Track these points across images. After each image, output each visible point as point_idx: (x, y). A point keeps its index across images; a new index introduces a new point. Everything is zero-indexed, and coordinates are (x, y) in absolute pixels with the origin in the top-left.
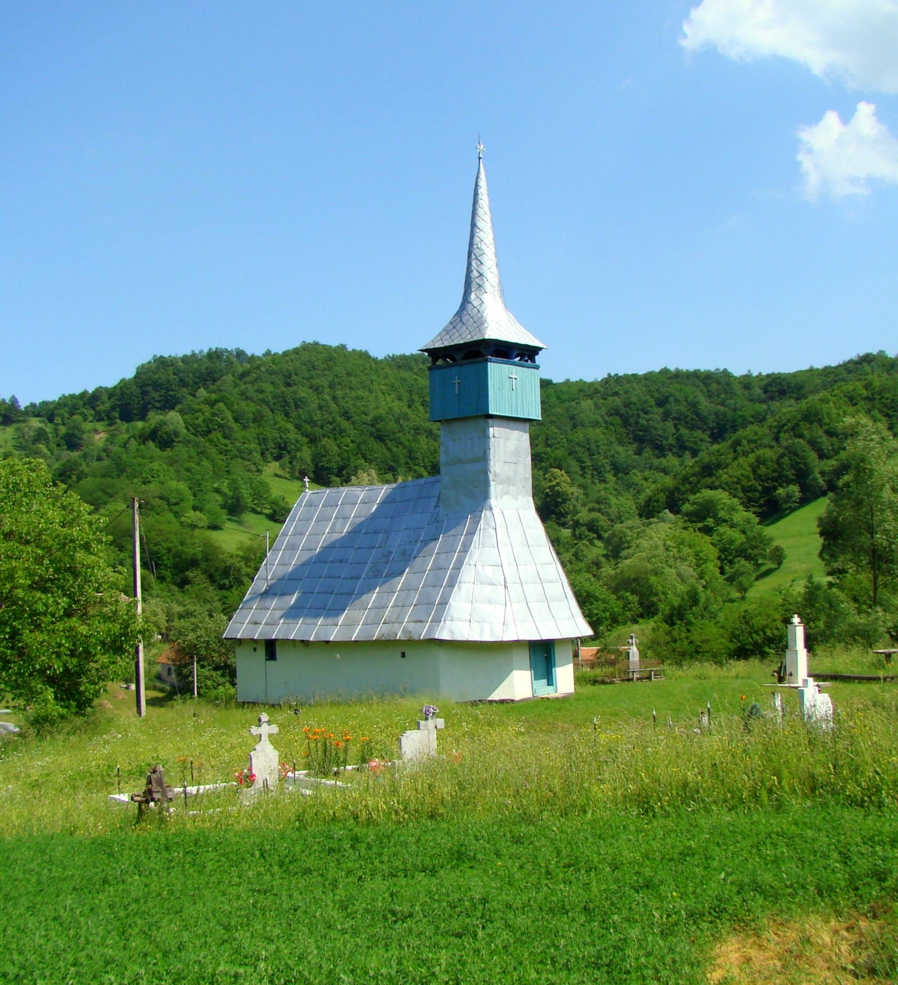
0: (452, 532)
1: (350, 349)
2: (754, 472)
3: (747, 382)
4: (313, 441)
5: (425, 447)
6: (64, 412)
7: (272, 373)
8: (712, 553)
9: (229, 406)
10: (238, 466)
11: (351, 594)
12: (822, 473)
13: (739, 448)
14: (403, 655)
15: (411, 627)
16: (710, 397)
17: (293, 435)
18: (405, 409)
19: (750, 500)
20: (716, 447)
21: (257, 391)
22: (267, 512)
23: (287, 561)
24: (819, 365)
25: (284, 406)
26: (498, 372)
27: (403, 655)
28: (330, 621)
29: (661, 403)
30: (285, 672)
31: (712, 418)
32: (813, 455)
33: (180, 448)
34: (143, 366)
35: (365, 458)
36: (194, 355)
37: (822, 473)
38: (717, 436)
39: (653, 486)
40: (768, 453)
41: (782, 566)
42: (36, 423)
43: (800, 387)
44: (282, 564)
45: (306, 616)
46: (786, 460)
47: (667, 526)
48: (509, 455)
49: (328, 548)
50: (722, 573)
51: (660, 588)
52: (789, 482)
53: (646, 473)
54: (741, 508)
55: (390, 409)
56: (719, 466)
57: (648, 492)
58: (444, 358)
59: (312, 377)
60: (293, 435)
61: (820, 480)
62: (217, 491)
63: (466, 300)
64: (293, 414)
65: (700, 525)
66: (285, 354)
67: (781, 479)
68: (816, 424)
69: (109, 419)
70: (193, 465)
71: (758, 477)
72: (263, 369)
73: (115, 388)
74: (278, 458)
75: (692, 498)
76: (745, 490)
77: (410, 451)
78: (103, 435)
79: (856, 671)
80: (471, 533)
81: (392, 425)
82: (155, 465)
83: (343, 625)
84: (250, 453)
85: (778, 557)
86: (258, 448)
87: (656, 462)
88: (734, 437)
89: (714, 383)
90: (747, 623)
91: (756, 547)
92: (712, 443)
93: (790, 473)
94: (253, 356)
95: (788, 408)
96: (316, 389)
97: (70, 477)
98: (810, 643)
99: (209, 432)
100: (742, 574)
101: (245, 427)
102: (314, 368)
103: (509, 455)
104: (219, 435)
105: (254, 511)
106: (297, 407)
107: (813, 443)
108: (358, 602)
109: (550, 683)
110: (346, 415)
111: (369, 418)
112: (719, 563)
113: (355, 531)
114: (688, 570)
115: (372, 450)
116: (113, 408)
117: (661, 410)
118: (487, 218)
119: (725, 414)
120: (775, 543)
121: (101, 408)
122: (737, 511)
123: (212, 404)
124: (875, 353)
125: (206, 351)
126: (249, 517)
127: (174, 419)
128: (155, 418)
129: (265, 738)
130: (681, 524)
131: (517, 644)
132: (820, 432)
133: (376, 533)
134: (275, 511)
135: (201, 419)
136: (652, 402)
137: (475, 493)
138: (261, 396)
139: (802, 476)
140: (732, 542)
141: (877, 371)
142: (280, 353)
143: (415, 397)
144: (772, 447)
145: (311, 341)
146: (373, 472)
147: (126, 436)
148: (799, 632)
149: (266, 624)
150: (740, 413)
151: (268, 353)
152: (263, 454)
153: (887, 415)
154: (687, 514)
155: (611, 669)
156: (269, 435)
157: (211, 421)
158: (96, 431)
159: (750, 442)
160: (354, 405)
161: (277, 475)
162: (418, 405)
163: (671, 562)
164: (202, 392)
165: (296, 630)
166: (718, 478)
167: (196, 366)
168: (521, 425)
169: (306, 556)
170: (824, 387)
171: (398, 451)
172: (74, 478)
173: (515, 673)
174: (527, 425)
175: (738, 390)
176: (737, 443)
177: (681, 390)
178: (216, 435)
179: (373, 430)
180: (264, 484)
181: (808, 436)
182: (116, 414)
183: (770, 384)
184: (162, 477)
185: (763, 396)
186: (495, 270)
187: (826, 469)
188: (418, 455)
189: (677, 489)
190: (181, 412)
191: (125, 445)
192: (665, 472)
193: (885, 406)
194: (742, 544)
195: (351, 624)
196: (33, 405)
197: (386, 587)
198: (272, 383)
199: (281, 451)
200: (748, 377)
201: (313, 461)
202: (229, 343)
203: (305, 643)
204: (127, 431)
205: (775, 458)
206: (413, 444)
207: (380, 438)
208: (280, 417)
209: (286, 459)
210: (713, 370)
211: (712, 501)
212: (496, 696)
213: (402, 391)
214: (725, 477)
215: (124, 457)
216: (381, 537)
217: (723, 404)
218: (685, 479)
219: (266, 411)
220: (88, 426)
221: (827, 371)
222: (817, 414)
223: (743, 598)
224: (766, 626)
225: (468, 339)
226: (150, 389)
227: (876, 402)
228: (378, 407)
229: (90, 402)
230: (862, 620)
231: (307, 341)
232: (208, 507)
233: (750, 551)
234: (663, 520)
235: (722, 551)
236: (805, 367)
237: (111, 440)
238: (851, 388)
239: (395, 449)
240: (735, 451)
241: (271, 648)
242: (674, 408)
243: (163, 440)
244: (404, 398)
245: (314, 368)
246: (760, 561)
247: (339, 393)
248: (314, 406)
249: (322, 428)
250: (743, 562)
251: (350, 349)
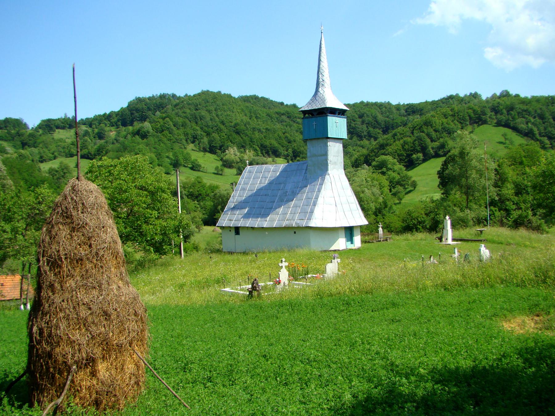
0: (313, 184)
2: (403, 147)
3: (398, 107)
4: (208, 134)
5: (258, 137)
7: (189, 104)
8: (386, 183)
9: (171, 119)
10: (177, 146)
12: (433, 148)
13: (396, 137)
14: (295, 233)
15: (299, 221)
16: (382, 114)
17: (199, 132)
18: (248, 120)
19: (401, 160)
20: (385, 136)
22: (190, 166)
23: (242, 195)
24: (430, 100)
25: (196, 119)
26: (332, 120)
27: (295, 233)
28: (263, 219)
29: (361, 117)
31: (383, 123)
32: (428, 140)
34: (131, 102)
35: (231, 142)
36: (153, 96)
37: (433, 148)
38: (385, 131)
39: (358, 154)
40: (409, 139)
41: (416, 189)
42: (84, 128)
43: (421, 110)
44: (240, 196)
45: (252, 217)
46: (417, 142)
47: (365, 171)
48: (335, 153)
49: (261, 189)
50: (390, 192)
53: (355, 148)
54: (397, 163)
56: (387, 145)
57: (356, 156)
58: (309, 114)
59: (207, 106)
60: (199, 132)
61: (432, 151)
62: (168, 157)
63: (317, 91)
64: (199, 123)
65: (380, 171)
66: (194, 96)
67: (415, 151)
69: (117, 125)
70: (157, 146)
71: (405, 150)
72: (185, 103)
73: (119, 111)
74: (193, 142)
75: (376, 159)
76: (399, 156)
77: (251, 139)
78: (114, 132)
79: (469, 237)
80: (321, 184)
81: (243, 127)
82: (141, 146)
84: (181, 140)
85: (414, 185)
86: (184, 137)
87: (359, 143)
88: (394, 132)
90: (410, 215)
93: (418, 148)
94: (179, 97)
95: (417, 119)
96: (209, 112)
97: (102, 152)
98: (453, 226)
99: (163, 131)
100: (399, 192)
102: (208, 102)
103: (335, 153)
104: (167, 132)
105: (185, 166)
107: (428, 135)
108: (274, 212)
109: (352, 243)
110: (223, 123)
111: (233, 124)
112: (389, 188)
113: (271, 183)
114: (376, 190)
115: (235, 139)
116: (118, 121)
117: (361, 120)
118: (325, 57)
120: (413, 179)
122: (396, 165)
123: (164, 119)
124: (454, 94)
125: (159, 94)
126: (182, 169)
127: (147, 125)
128: (137, 125)
129: (284, 267)
130: (371, 170)
131: (341, 228)
133: (280, 184)
134: (193, 166)
135: (159, 125)
136: (357, 116)
138: (185, 115)
139: (424, 149)
140: (394, 178)
141: (455, 102)
142: (192, 95)
144: (410, 137)
146: (235, 148)
147: (125, 133)
149: (235, 220)
150: (396, 121)
151: (186, 95)
152: (186, 140)
153: (460, 123)
154: (374, 166)
155: (372, 237)
156: (189, 132)
157: (164, 126)
158: (111, 131)
159: (401, 134)
160: (226, 119)
161: (193, 150)
162: (254, 118)
163: (369, 187)
164: (158, 113)
165: (249, 223)
166: (387, 150)
167: (154, 101)
168: (340, 141)
169: (250, 193)
170: (432, 110)
172: (104, 152)
173: (340, 239)
175: (394, 111)
176: (395, 135)
177: (369, 111)
178: (166, 132)
180: (188, 154)
181: (426, 132)
182: (120, 123)
183: (408, 108)
184: (144, 152)
185: (405, 114)
186: (328, 78)
187: (434, 146)
188: (255, 140)
189: (369, 155)
190: (150, 122)
191: (125, 137)
192: (363, 147)
193: (460, 119)
194: (399, 179)
195: (273, 220)
196: (82, 120)
197: (286, 206)
198: (190, 109)
199: (194, 139)
201: (209, 143)
202: (169, 91)
203: (253, 228)
204: (125, 131)
205: (412, 141)
207: (238, 133)
208: (194, 125)
209: (197, 142)
212: (333, 248)
213: (246, 112)
215: (126, 143)
216: (282, 185)
217: (388, 117)
218: (372, 151)
219: (187, 121)
220: (107, 129)
221: (433, 103)
222: (430, 122)
224: (418, 217)
226: (134, 112)
227: (456, 117)
228: (236, 119)
229: (108, 117)
231: (204, 90)
233: (402, 182)
234: (363, 169)
235: (390, 182)
236: (424, 101)
237: (118, 133)
238: (445, 111)
239: (244, 138)
240: (394, 138)
241: (237, 230)
242: (366, 119)
245: (208, 102)
246: (406, 187)
247: (219, 113)
248: (208, 119)
250: (399, 187)
251: (223, 93)
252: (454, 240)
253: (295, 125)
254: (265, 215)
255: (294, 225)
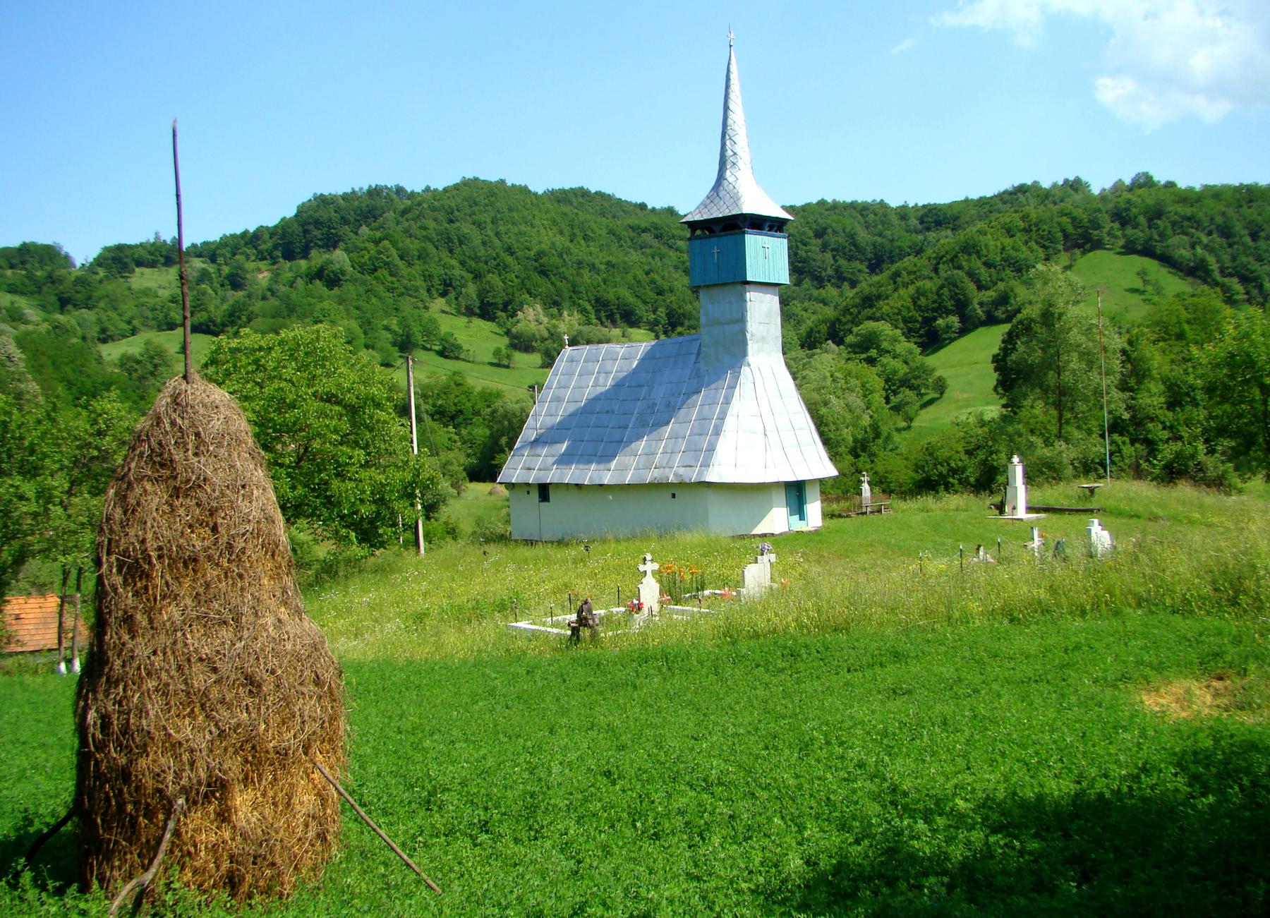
0: (713, 386)
1: (509, 184)
2: (915, 303)
4: (477, 276)
5: (588, 281)
6: (226, 252)
7: (434, 209)
8: (878, 383)
9: (394, 243)
10: (407, 304)
11: (621, 441)
12: (981, 304)
14: (674, 496)
15: (682, 471)
16: (867, 228)
17: (458, 272)
18: (568, 244)
19: (910, 330)
20: (876, 278)
21: (421, 228)
22: (437, 348)
24: (975, 195)
25: (449, 242)
26: (754, 243)
27: (674, 496)
28: (602, 466)
29: (819, 234)
30: (556, 514)
31: (869, 249)
32: (971, 287)
33: (349, 287)
34: (303, 204)
36: (354, 192)
37: (981, 304)
38: (875, 266)
39: (814, 318)
40: (928, 285)
41: (945, 395)
42: (198, 264)
43: (956, 218)
44: (549, 414)
45: (578, 462)
46: (945, 291)
47: (830, 357)
49: (594, 401)
50: (887, 402)
51: (830, 419)
52: (949, 313)
53: (806, 304)
54: (903, 338)
55: (553, 244)
56: (879, 297)
57: (809, 323)
58: (702, 229)
59: (474, 213)
60: (458, 272)
61: (979, 311)
62: (387, 328)
63: (721, 177)
64: (457, 250)
65: (864, 356)
66: (446, 190)
67: (941, 310)
68: (974, 256)
69: (272, 258)
70: (361, 303)
71: (919, 309)
73: (276, 227)
74: (444, 294)
75: (855, 329)
76: (905, 321)
77: (574, 286)
78: (266, 274)
79: (1066, 504)
80: (732, 387)
81: (555, 260)
83: (616, 470)
84: (417, 290)
85: (941, 387)
86: (424, 285)
87: (815, 293)
88: (894, 268)
89: (871, 214)
90: (931, 454)
91: (919, 377)
92: (870, 274)
93: (949, 304)
94: (412, 192)
95: (945, 239)
96: (479, 225)
97: (239, 318)
98: (1029, 478)
99: (376, 270)
100: (907, 403)
101: (410, 265)
102: (476, 204)
104: (385, 272)
105: (425, 348)
106: (461, 243)
107: (971, 275)
109: (802, 518)
110: (510, 250)
111: (532, 253)
112: (884, 394)
113: (618, 385)
114: (855, 400)
115: (538, 286)
116: (275, 247)
117: (819, 241)
118: (739, 101)
119: (882, 245)
120: (937, 374)
121: (263, 247)
123: (377, 242)
124: (1029, 183)
125: (366, 188)
127: (340, 257)
128: (318, 258)
129: (649, 573)
130: (845, 355)
131: (777, 484)
132: (979, 264)
134: (445, 348)
136: (811, 234)
137: (734, 350)
138: (424, 233)
139: (961, 307)
140: (895, 372)
141: (1032, 201)
142: (441, 189)
143: (576, 231)
144: (931, 278)
145: (471, 177)
146: (538, 307)
147: (290, 275)
148: (1019, 470)
149: (540, 469)
150: (898, 244)
151: (427, 189)
152: (428, 291)
154: (851, 346)
157: (378, 259)
158: (259, 270)
159: (909, 273)
161: (443, 312)
162: (580, 239)
163: (839, 392)
164: (364, 230)
165: (570, 474)
168: (772, 288)
169: (572, 408)
170: (980, 218)
171: (562, 285)
172: (244, 318)
173: (775, 510)
174: (777, 289)
175: (895, 221)
176: (897, 275)
178: (382, 273)
179: (536, 264)
180: (432, 321)
181: (966, 268)
185: (920, 227)
186: (747, 149)
187: (985, 300)
188: (582, 289)
189: (838, 320)
190: (347, 250)
191: (292, 284)
194: (906, 374)
196: (194, 246)
198: (435, 220)
199: (446, 288)
200: (905, 207)
201: (479, 296)
202: (388, 178)
206: (577, 279)
208: (445, 255)
209: (452, 295)
210: (869, 201)
211: (875, 333)
212: (759, 530)
213: (563, 226)
214: (886, 309)
215: (294, 296)
216: (644, 391)
217: (880, 235)
218: (846, 311)
219: (431, 248)
220: (251, 265)
221: (982, 202)
222: (974, 246)
223: (909, 428)
224: (950, 458)
225: (727, 213)
226: (311, 227)
227: (1033, 233)
228: (540, 242)
229: (251, 240)
230: (1047, 452)
232: (378, 345)
233: (913, 381)
234: (826, 352)
235: (887, 381)
237: (276, 276)
238: (1008, 220)
239: (558, 283)
240: (895, 283)
241: (544, 491)
242: (832, 239)
243: (333, 280)
244: (566, 233)
245: (476, 204)
247: (502, 229)
248: (477, 242)
249: (486, 263)
250: (908, 392)
251: (509, 184)
252: (1030, 509)
253: (672, 254)
254: (606, 458)
255: (671, 479)
